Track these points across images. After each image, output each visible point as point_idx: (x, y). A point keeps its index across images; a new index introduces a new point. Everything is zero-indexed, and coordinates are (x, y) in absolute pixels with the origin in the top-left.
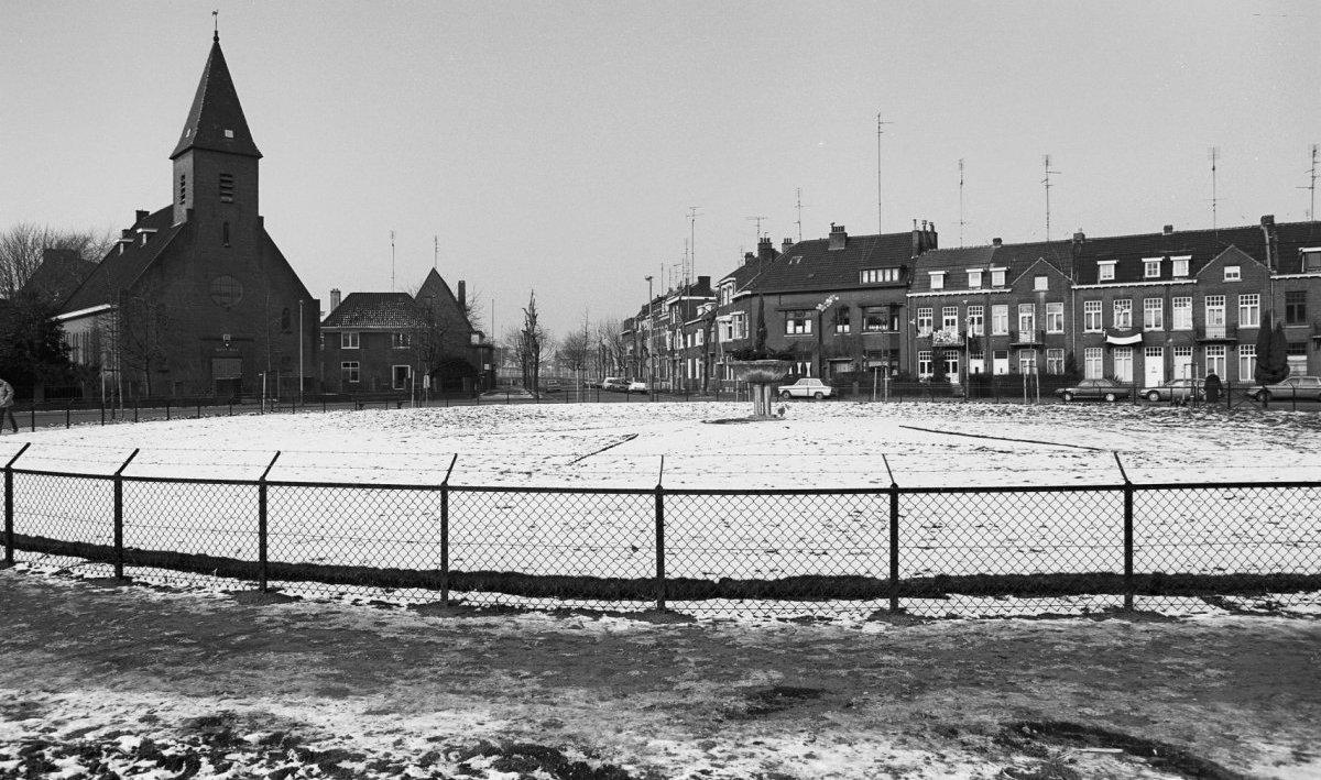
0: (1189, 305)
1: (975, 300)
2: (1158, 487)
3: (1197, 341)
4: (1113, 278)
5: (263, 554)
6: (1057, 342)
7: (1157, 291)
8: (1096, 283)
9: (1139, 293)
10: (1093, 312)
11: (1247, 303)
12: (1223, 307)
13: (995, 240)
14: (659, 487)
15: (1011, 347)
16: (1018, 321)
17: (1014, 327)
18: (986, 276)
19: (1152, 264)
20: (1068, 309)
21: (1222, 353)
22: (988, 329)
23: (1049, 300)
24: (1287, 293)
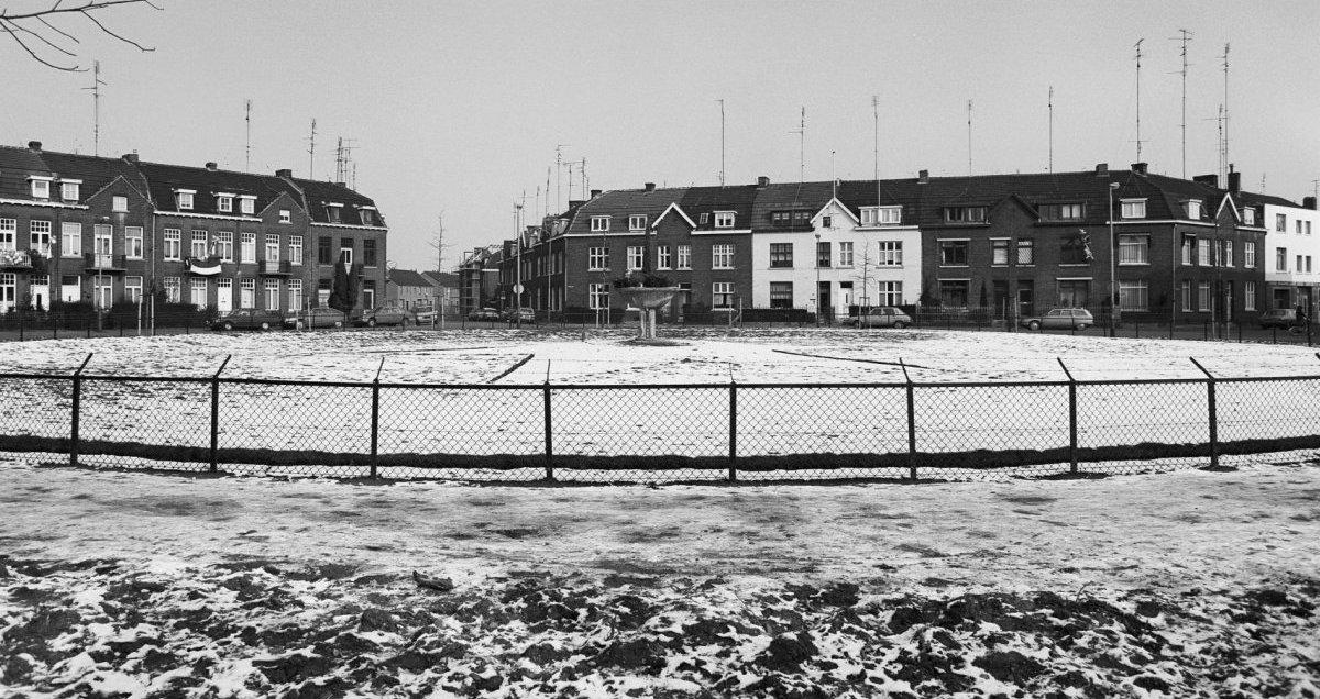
0: (254, 241)
1: (40, 214)
2: (782, 386)
3: (260, 275)
4: (191, 207)
5: (214, 441)
6: (135, 269)
7: (230, 225)
8: (176, 210)
9: (214, 226)
10: (172, 240)
11: (38, 230)
12: (278, 246)
13: (31, 144)
14: (547, 383)
15: (84, 270)
16: (93, 244)
17: (88, 250)
18: (56, 190)
19: (225, 198)
20: (147, 236)
21: (12, 282)
22: (57, 249)
23: (128, 222)
24: (321, 238)
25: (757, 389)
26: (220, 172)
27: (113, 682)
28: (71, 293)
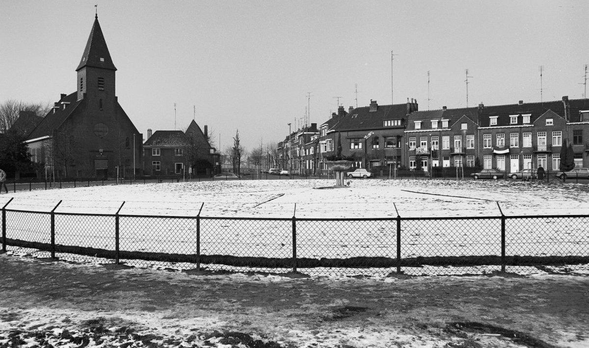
0: (530, 136)
1: (435, 134)
2: (516, 217)
3: (534, 152)
4: (496, 124)
6: (471, 153)
7: (516, 130)
8: (489, 126)
9: (508, 131)
10: (487, 139)
11: (556, 135)
12: (545, 137)
13: (443, 107)
15: (451, 155)
16: (454, 143)
17: (452, 146)
18: (440, 123)
19: (514, 118)
20: (476, 138)
21: (545, 158)
22: (441, 147)
23: (468, 134)
24: (574, 131)
25: (534, 219)
26: (525, 104)
27: (572, 345)
28: (446, 163)
